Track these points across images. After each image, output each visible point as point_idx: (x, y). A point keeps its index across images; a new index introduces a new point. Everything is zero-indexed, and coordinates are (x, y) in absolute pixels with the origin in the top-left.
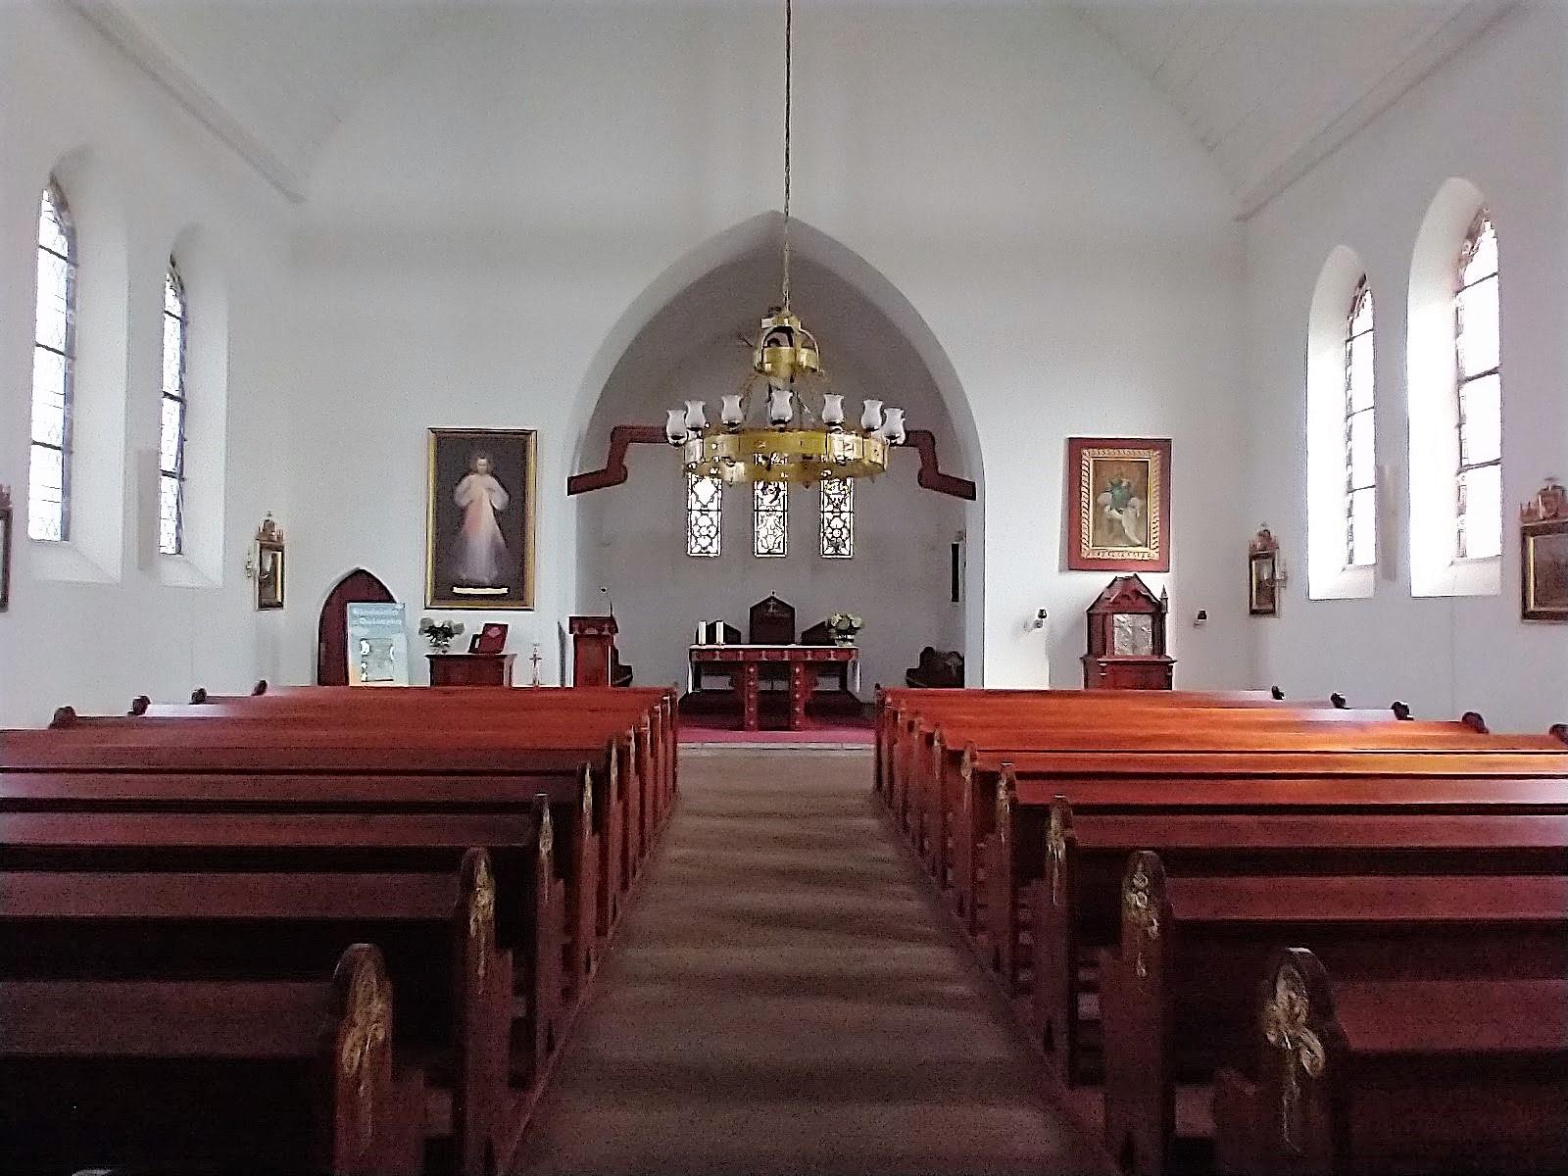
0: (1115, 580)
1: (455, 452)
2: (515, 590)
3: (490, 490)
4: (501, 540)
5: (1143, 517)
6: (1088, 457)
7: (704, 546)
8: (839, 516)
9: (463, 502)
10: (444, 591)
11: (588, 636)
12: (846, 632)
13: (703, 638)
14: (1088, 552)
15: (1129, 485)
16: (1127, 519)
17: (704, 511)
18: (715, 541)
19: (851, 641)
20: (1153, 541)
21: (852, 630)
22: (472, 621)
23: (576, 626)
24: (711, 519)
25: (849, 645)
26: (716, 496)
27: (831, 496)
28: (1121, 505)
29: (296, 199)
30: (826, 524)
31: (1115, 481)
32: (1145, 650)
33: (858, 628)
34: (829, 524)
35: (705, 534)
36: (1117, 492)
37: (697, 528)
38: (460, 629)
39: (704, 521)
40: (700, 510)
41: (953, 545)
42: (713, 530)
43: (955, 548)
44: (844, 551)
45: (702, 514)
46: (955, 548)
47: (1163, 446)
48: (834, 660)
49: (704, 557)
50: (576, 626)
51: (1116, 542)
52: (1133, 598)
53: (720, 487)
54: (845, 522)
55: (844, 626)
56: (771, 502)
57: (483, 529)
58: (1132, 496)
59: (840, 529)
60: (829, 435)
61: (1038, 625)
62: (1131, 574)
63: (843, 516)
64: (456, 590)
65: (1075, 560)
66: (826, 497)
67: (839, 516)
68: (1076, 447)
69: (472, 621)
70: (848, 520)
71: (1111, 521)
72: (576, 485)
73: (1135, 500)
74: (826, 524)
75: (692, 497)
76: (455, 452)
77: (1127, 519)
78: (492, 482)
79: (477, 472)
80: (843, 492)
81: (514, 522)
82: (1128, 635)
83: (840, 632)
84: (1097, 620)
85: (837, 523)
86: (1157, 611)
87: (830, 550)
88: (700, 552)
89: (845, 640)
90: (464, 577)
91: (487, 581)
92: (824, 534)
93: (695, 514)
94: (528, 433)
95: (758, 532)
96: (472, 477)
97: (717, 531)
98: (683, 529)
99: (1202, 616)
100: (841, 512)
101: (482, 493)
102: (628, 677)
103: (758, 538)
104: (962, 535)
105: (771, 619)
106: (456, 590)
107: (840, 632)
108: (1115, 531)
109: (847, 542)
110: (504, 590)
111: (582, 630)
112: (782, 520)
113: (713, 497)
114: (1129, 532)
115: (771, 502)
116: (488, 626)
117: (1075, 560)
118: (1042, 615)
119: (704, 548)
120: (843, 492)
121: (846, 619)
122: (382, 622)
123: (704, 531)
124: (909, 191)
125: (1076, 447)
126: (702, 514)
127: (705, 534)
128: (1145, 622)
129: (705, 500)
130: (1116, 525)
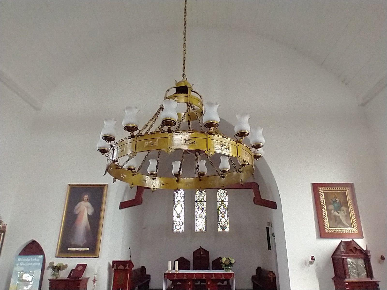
0: (341, 242)
1: (76, 193)
2: (92, 249)
3: (88, 207)
4: (89, 227)
5: (348, 215)
6: (322, 192)
7: (178, 229)
8: (224, 218)
9: (77, 212)
10: (64, 250)
11: (120, 269)
12: (228, 266)
13: (170, 268)
14: (328, 228)
15: (340, 201)
16: (341, 215)
17: (178, 216)
18: (182, 227)
19: (231, 269)
20: (354, 225)
21: (231, 264)
22: (72, 263)
23: (115, 265)
24: (181, 219)
25: (231, 272)
26: (182, 211)
27: (221, 211)
28: (338, 209)
29: (37, 109)
30: (219, 221)
31: (334, 200)
32: (364, 277)
33: (233, 264)
34: (221, 220)
35: (179, 225)
36: (335, 205)
37: (176, 222)
38: (66, 266)
39: (178, 220)
40: (177, 216)
41: (267, 227)
42: (181, 223)
43: (268, 229)
44: (226, 230)
45: (178, 218)
46: (268, 229)
47: (350, 186)
48: (224, 278)
49: (178, 234)
50: (115, 265)
51: (339, 226)
52: (351, 249)
53: (184, 208)
54: (226, 219)
55: (227, 263)
56: (201, 213)
57: (83, 222)
58: (342, 206)
59: (225, 222)
60: (209, 135)
61: (311, 263)
62: (351, 240)
63: (220, 200)
64: (69, 249)
65: (322, 234)
66: (219, 211)
67: (224, 218)
68: (316, 187)
69: (72, 263)
70: (227, 219)
71: (335, 216)
72: (123, 205)
73: (343, 208)
74: (219, 221)
75: (175, 212)
76: (76, 193)
77: (341, 215)
78: (88, 204)
79: (83, 200)
80: (225, 209)
81: (95, 221)
82: (355, 269)
83: (226, 265)
84: (337, 261)
85: (223, 220)
86: (365, 256)
87: (221, 230)
88: (177, 231)
89: (228, 269)
90: (73, 243)
91: (81, 245)
92: (219, 224)
93: (175, 218)
94: (104, 185)
95: (196, 223)
96: (82, 203)
97: (183, 223)
98: (171, 223)
99: (383, 258)
100: (225, 216)
101: (85, 209)
102: (149, 279)
103: (196, 226)
104: (270, 224)
105: (201, 258)
106: (69, 249)
107: (226, 265)
108: (336, 221)
109: (227, 227)
110: (88, 249)
111: (117, 267)
112: (204, 219)
113: (181, 211)
114: (343, 220)
115: (201, 213)
116: (79, 265)
117: (322, 234)
118: (313, 259)
119: (178, 230)
120: (225, 209)
121: (228, 260)
122: (31, 264)
123: (178, 224)
124: (246, 101)
125: (316, 187)
126: (178, 218)
127: (179, 225)
128: (361, 262)
129: (179, 212)
130: (337, 218)
